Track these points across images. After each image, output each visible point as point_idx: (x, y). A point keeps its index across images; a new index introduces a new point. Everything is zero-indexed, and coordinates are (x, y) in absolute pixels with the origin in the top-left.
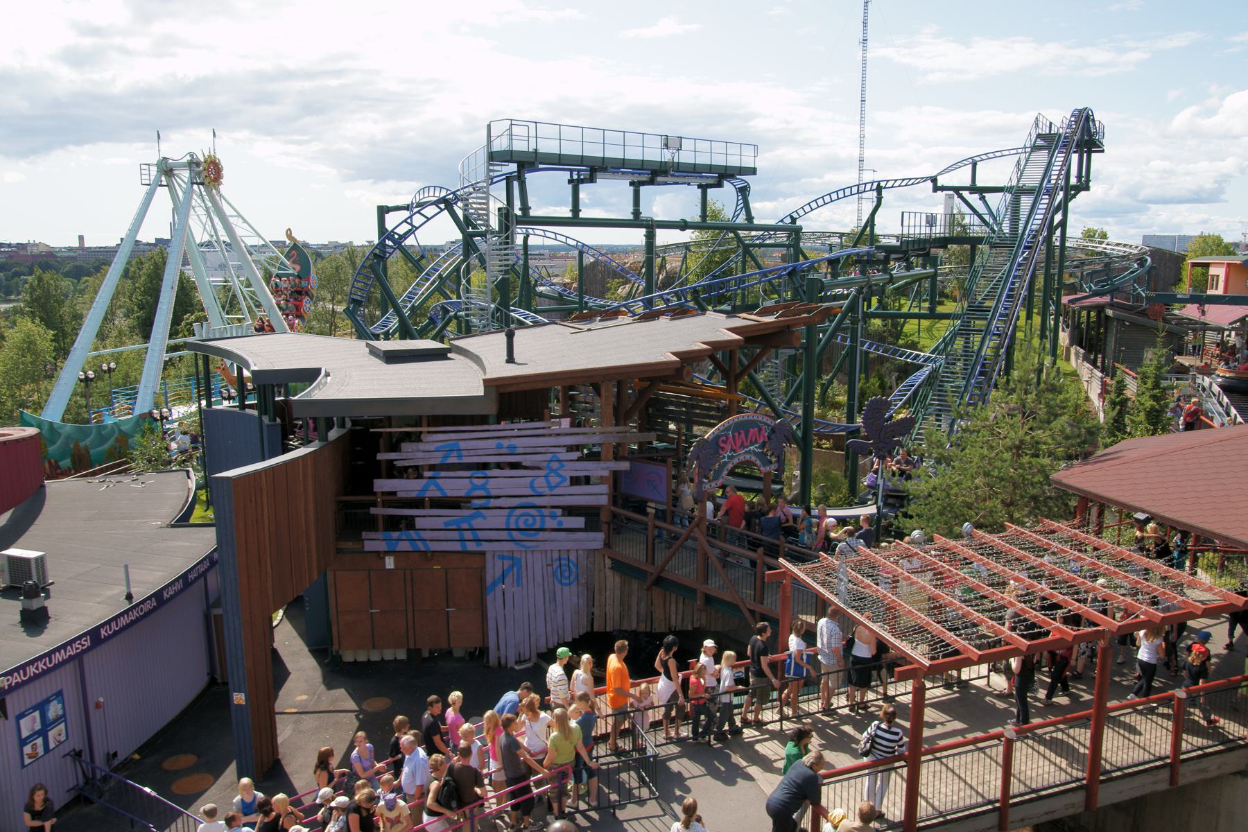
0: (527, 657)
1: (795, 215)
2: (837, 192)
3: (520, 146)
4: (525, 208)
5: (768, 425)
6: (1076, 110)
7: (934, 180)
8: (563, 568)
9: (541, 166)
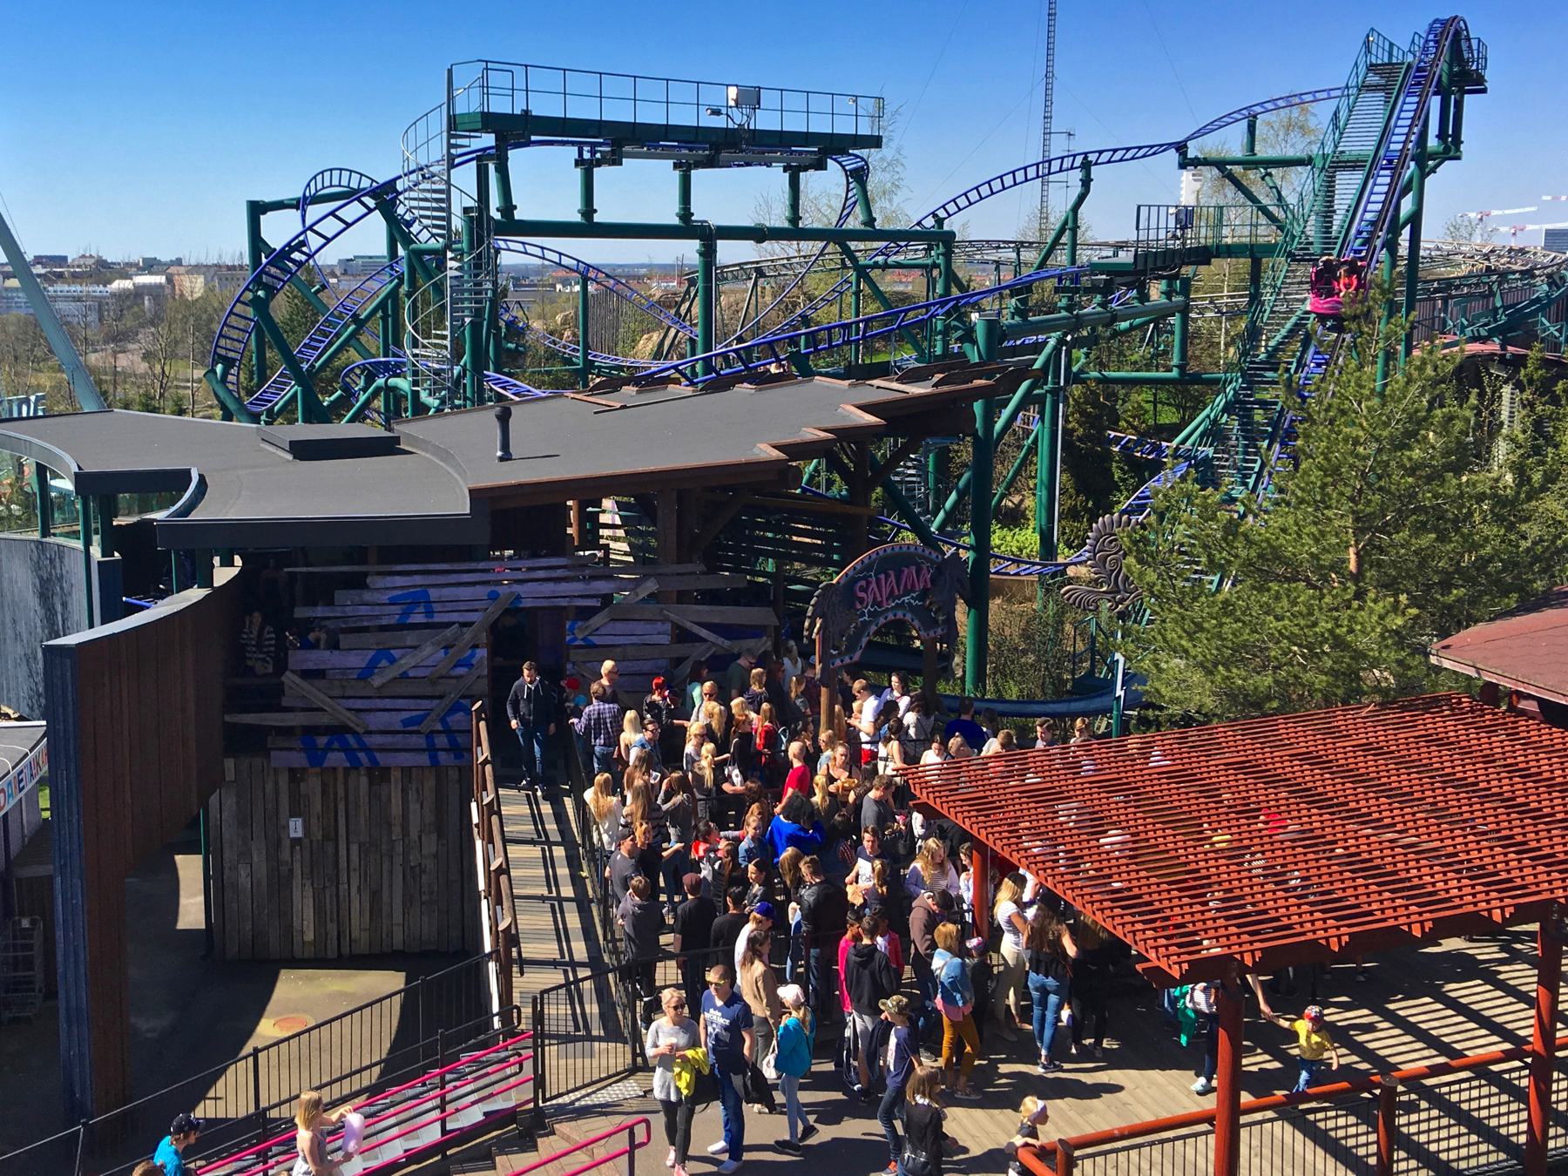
1: (941, 213)
2: (1025, 169)
3: (499, 106)
4: (508, 207)
6: (1436, 21)
7: (1181, 148)
9: (533, 138)
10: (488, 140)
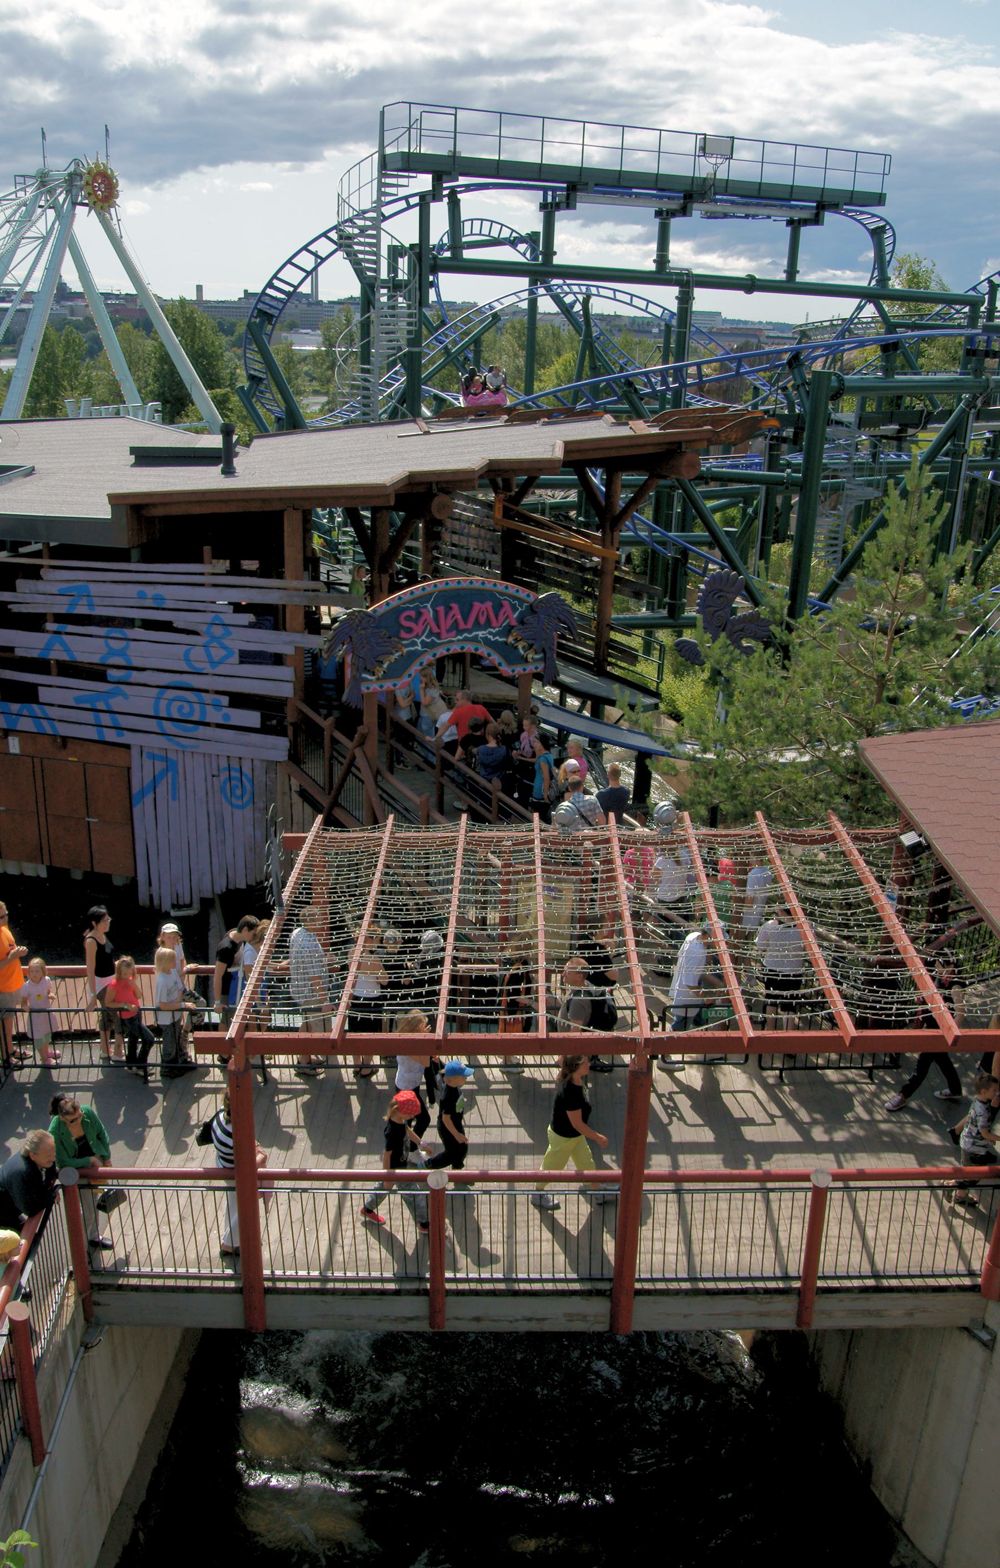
0: (187, 901)
5: (521, 601)
8: (233, 782)
10: (424, 182)
